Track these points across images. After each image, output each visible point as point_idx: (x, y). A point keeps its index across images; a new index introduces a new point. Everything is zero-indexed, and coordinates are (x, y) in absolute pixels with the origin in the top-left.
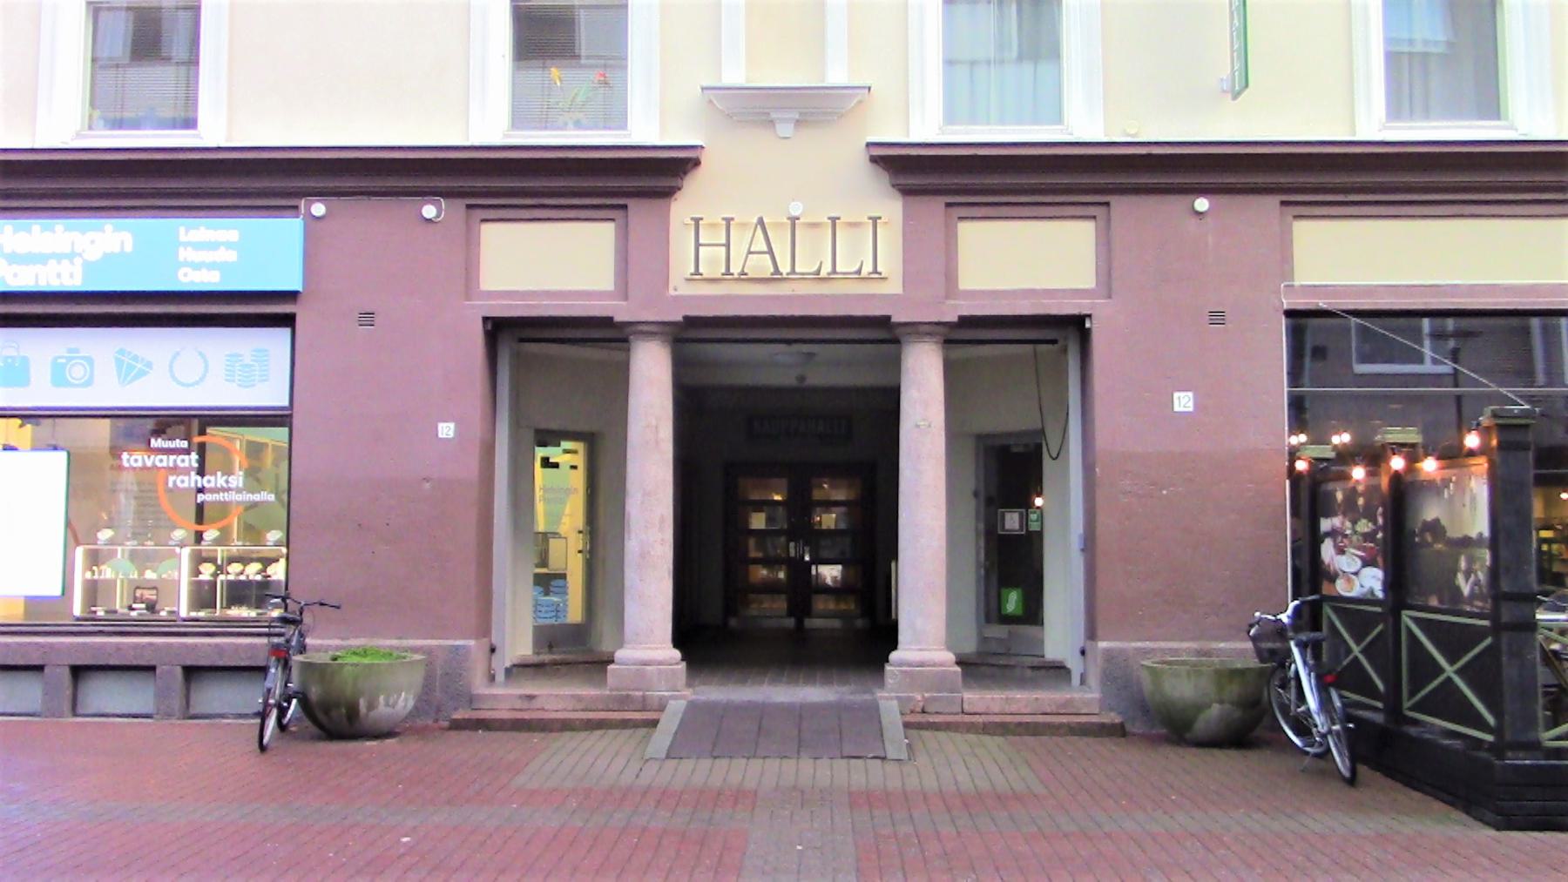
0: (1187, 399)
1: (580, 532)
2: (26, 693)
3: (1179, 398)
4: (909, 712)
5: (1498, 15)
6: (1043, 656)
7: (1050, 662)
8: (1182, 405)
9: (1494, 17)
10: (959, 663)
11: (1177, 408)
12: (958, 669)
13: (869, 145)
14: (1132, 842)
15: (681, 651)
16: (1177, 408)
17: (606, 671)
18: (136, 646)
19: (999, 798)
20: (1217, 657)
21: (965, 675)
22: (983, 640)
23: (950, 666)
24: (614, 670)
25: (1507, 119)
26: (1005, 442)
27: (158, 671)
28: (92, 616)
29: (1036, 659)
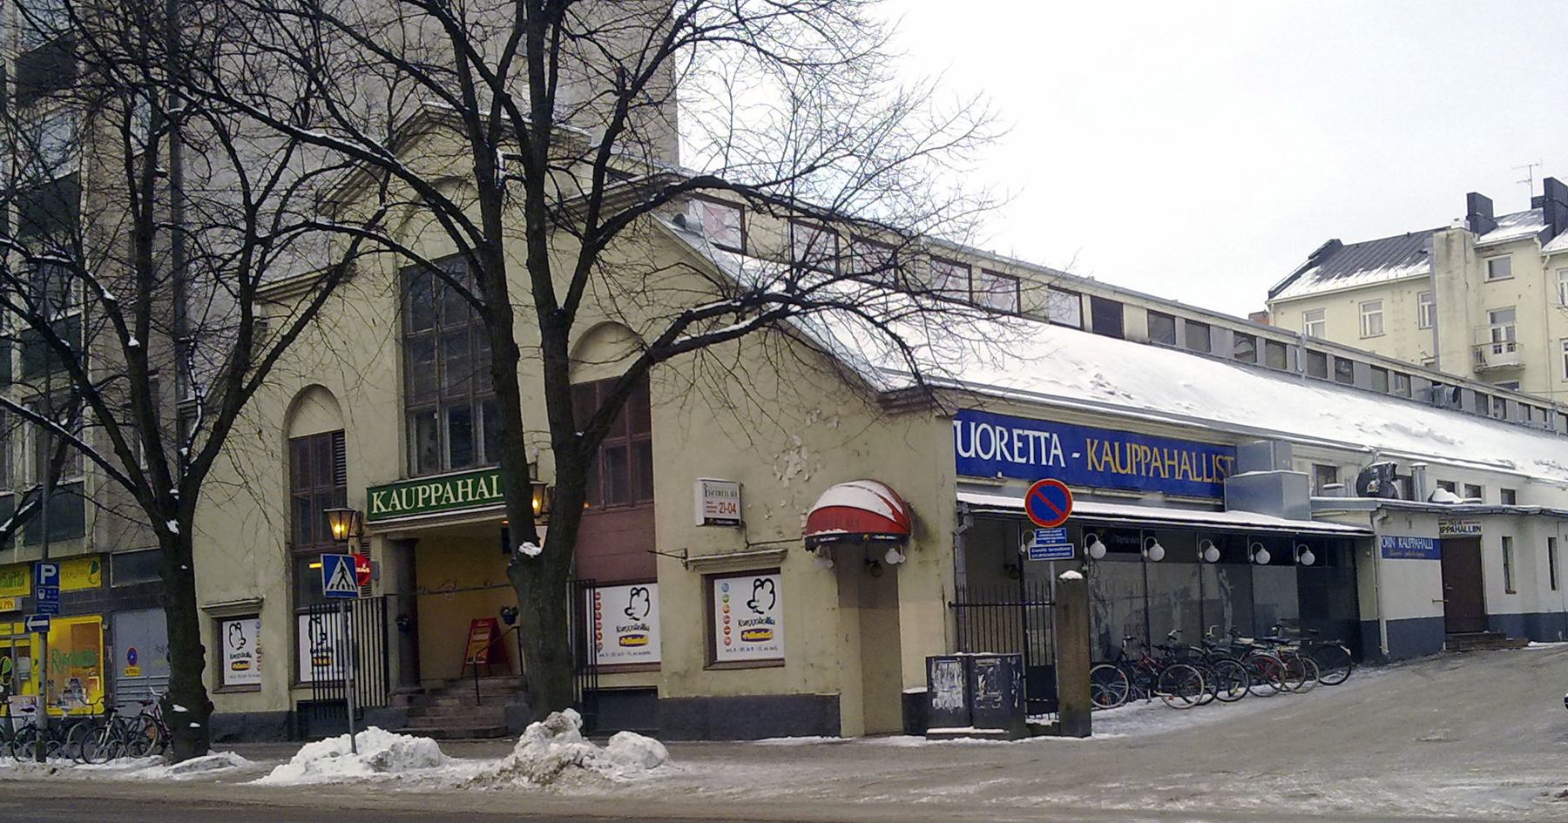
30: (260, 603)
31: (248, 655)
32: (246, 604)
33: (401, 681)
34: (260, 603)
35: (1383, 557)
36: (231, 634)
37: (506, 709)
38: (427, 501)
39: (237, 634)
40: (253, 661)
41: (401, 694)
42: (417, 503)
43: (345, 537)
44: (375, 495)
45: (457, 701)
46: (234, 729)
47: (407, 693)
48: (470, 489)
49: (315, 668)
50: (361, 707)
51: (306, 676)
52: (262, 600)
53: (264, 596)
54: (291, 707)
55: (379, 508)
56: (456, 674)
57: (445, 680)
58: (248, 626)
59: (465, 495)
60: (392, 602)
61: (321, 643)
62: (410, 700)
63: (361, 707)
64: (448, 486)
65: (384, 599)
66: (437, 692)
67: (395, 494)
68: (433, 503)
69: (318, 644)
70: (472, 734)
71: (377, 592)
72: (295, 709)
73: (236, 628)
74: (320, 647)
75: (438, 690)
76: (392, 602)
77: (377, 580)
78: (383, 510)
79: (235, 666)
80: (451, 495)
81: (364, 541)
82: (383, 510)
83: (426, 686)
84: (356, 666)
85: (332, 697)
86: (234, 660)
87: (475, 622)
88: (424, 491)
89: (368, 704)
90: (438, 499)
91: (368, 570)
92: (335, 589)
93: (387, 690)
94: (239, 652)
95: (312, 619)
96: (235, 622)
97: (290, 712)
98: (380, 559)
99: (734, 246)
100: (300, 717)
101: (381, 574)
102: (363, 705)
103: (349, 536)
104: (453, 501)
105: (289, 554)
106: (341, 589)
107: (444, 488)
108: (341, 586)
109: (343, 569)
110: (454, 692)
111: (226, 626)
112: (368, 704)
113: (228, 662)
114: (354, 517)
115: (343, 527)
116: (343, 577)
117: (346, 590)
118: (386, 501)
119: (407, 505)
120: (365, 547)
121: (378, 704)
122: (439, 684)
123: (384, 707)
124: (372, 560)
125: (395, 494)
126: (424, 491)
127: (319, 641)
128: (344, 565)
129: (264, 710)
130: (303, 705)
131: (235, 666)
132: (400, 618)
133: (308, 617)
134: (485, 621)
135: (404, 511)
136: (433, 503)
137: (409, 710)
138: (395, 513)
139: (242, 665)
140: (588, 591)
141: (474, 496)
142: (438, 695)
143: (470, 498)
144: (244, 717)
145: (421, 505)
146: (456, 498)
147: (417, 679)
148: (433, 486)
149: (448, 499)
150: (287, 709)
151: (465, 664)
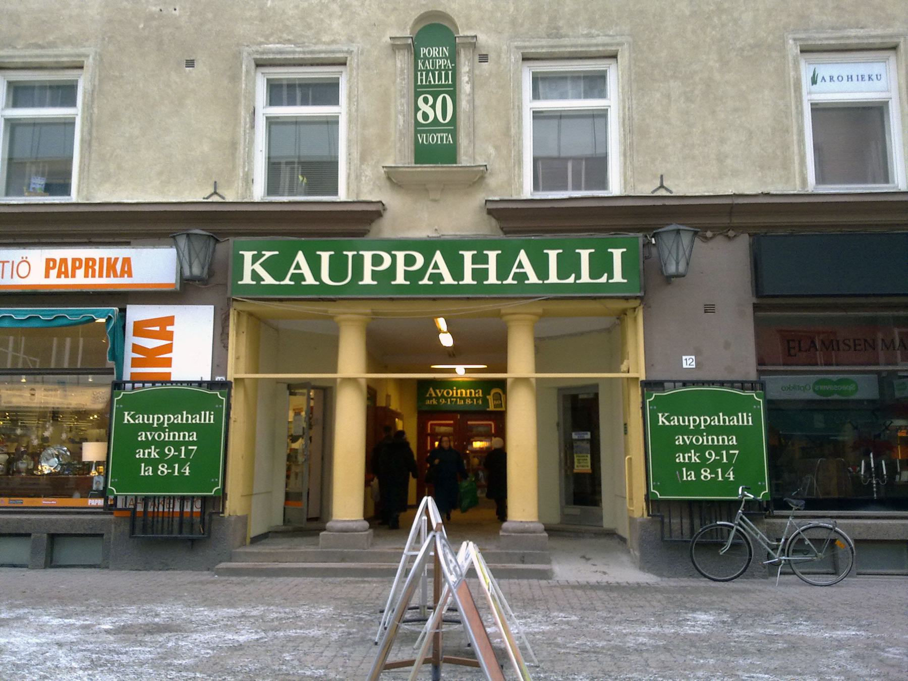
0: (691, 360)
1: (202, 378)
2: (18, 550)
3: (686, 359)
4: (290, 427)
5: (885, 119)
6: (602, 527)
7: (606, 530)
8: (688, 364)
9: (882, 122)
10: (546, 530)
11: (685, 366)
12: (546, 534)
13: (487, 62)
14: (553, 588)
15: (369, 523)
16: (685, 366)
17: (319, 535)
18: (51, 521)
19: (540, 587)
20: (361, 619)
21: (550, 536)
22: (564, 515)
23: (541, 533)
24: (323, 535)
25: (894, 182)
26: (574, 392)
27: (104, 537)
28: (450, 562)
29: (596, 528)
119: (331, 278)
148: (400, 256)
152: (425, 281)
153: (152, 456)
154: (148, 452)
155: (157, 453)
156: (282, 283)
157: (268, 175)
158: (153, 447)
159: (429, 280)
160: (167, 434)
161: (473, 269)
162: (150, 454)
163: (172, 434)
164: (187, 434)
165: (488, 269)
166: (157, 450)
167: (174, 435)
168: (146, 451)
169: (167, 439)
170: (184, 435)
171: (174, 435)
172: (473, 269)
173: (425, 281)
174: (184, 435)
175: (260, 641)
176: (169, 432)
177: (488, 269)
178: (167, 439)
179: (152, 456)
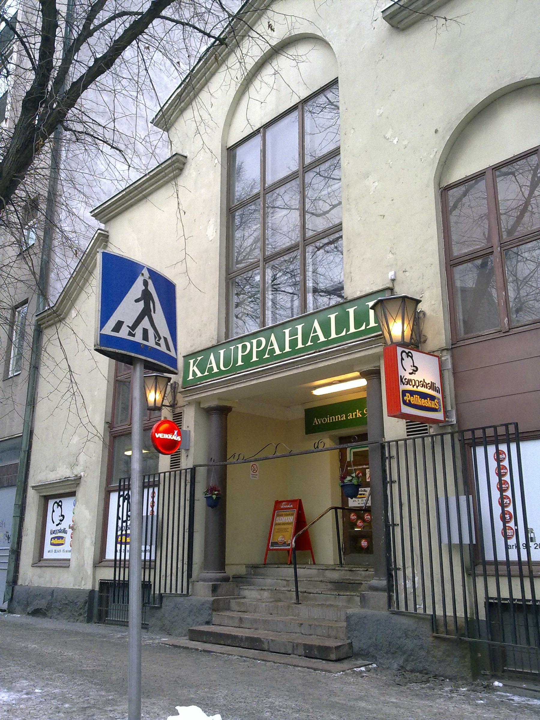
30: (78, 480)
31: (65, 531)
32: (65, 481)
33: (206, 566)
34: (78, 480)
35: (531, 542)
36: (53, 511)
37: (348, 618)
38: (247, 358)
39: (58, 510)
40: (67, 537)
41: (204, 580)
42: (236, 361)
43: (159, 404)
44: (192, 361)
45: (266, 594)
46: (42, 604)
47: (210, 580)
48: (300, 336)
49: (119, 546)
50: (160, 594)
51: (110, 555)
52: (80, 478)
53: (82, 474)
54: (94, 585)
55: (194, 373)
56: (258, 559)
57: (247, 566)
58: (67, 503)
59: (293, 343)
60: (201, 473)
61: (126, 521)
62: (215, 589)
63: (160, 594)
64: (273, 338)
65: (193, 470)
66: (239, 579)
67: (212, 357)
68: (255, 359)
69: (123, 522)
70: (301, 651)
71: (186, 463)
72: (97, 588)
73: (59, 505)
74: (124, 524)
75: (240, 577)
76: (201, 473)
77: (187, 450)
78: (199, 374)
79: (53, 541)
80: (276, 347)
81: (178, 411)
82: (199, 374)
83: (230, 571)
84: (159, 545)
85: (122, 579)
86: (54, 535)
87: (278, 503)
88: (244, 347)
89: (168, 591)
90: (260, 354)
91: (179, 438)
92: (123, 333)
93: (190, 576)
94: (59, 528)
95: (119, 496)
96: (58, 500)
97: (92, 592)
98: (192, 428)
99: (519, 163)
100: (101, 597)
101: (192, 443)
102: (162, 591)
103: (163, 405)
104: (278, 352)
105: (108, 434)
106: (138, 338)
107: (268, 340)
108: (139, 332)
109: (146, 296)
110: (258, 580)
111: (51, 503)
112: (168, 591)
113: (48, 537)
114: (169, 388)
115: (158, 393)
116: (146, 312)
117: (151, 343)
118: (202, 367)
119: (224, 367)
120: (178, 417)
121: (173, 592)
122: (242, 570)
123: (184, 595)
124: (184, 428)
125: (212, 357)
126: (244, 347)
127: (125, 519)
128: (151, 288)
129: (71, 586)
130: (104, 584)
131: (53, 541)
132: (210, 490)
133: (117, 494)
134: (288, 502)
135: (221, 372)
136: (255, 359)
137: (214, 601)
138: (212, 375)
139: (58, 541)
140: (480, 451)
141: (304, 342)
142: (242, 582)
143: (300, 345)
144: (52, 592)
145: (240, 363)
146: (282, 348)
147: (221, 565)
148: (254, 342)
149: (273, 351)
150: (89, 587)
151: (268, 549)
152: (266, 356)
153: (358, 416)
154: (355, 414)
155: (360, 414)
156: (204, 375)
157: (175, 310)
158: (357, 411)
159: (268, 355)
160: (328, 418)
161: (257, 351)
162: (356, 415)
163: (331, 418)
164: (339, 416)
165: (274, 348)
166: (360, 412)
167: (333, 418)
168: (354, 414)
169: (329, 422)
170: (338, 417)
171: (333, 418)
172: (257, 351)
173: (266, 356)
174: (338, 417)
175: (366, 569)
176: (330, 417)
177: (274, 348)
178: (329, 422)
179: (358, 416)
